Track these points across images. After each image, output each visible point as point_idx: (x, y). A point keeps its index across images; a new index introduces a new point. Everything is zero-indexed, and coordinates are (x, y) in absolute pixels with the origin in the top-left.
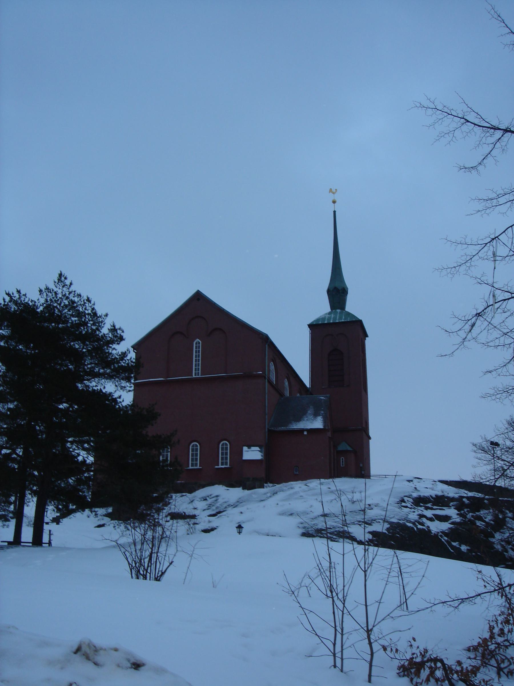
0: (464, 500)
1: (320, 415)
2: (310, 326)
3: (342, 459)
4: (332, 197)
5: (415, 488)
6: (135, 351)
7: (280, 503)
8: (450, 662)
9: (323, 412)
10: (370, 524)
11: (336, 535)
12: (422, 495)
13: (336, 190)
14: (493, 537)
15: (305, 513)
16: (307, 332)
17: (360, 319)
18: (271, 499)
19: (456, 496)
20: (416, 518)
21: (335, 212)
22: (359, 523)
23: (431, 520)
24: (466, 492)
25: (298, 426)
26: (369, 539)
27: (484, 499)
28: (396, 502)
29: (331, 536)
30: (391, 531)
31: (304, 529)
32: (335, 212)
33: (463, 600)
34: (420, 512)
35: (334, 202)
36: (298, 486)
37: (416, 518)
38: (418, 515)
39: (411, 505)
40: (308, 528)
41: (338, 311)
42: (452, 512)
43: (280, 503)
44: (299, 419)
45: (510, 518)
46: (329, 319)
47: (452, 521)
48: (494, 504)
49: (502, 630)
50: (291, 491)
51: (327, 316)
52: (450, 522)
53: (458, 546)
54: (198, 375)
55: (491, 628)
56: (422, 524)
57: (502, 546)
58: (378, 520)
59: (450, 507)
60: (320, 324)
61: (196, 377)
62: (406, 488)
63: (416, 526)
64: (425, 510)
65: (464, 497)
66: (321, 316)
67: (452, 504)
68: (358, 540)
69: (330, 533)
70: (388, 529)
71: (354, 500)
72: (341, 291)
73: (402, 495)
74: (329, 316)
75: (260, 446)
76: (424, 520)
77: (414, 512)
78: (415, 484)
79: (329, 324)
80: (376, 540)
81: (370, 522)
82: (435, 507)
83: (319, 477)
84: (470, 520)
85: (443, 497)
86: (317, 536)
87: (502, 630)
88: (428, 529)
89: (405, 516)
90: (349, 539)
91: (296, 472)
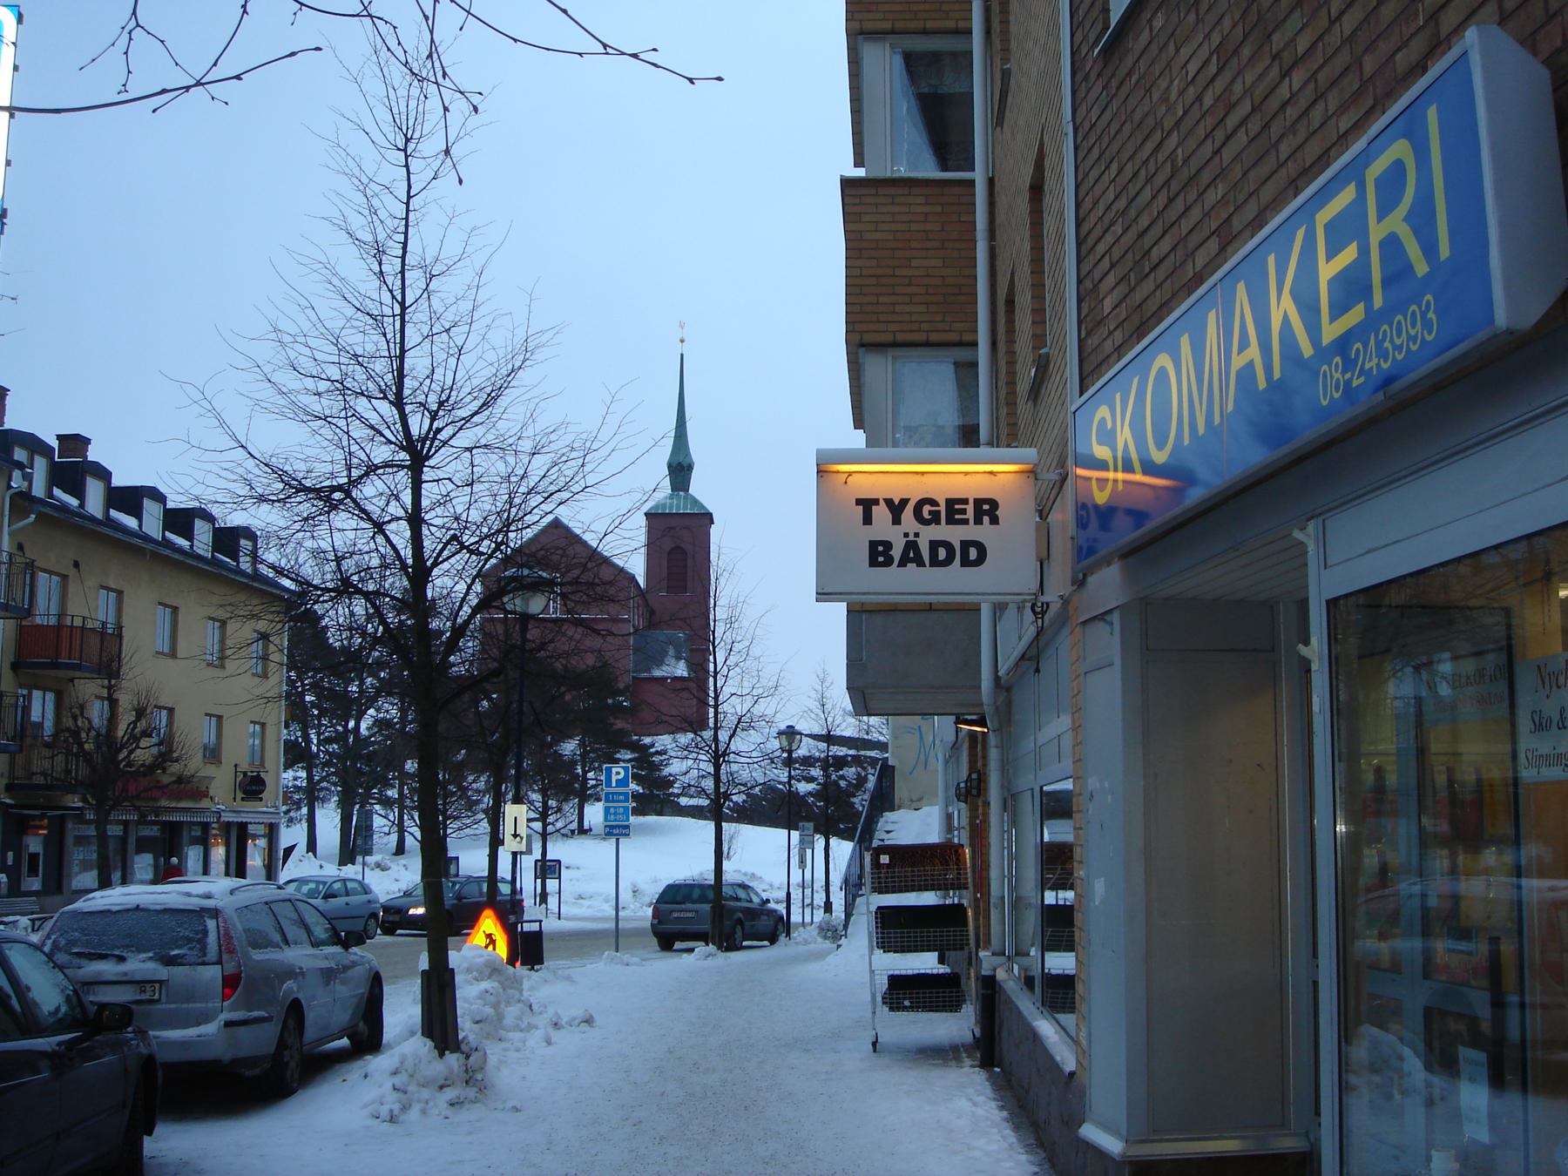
21: (682, 355)
27: (847, 756)
32: (682, 355)
35: (682, 341)
46: (671, 507)
51: (668, 501)
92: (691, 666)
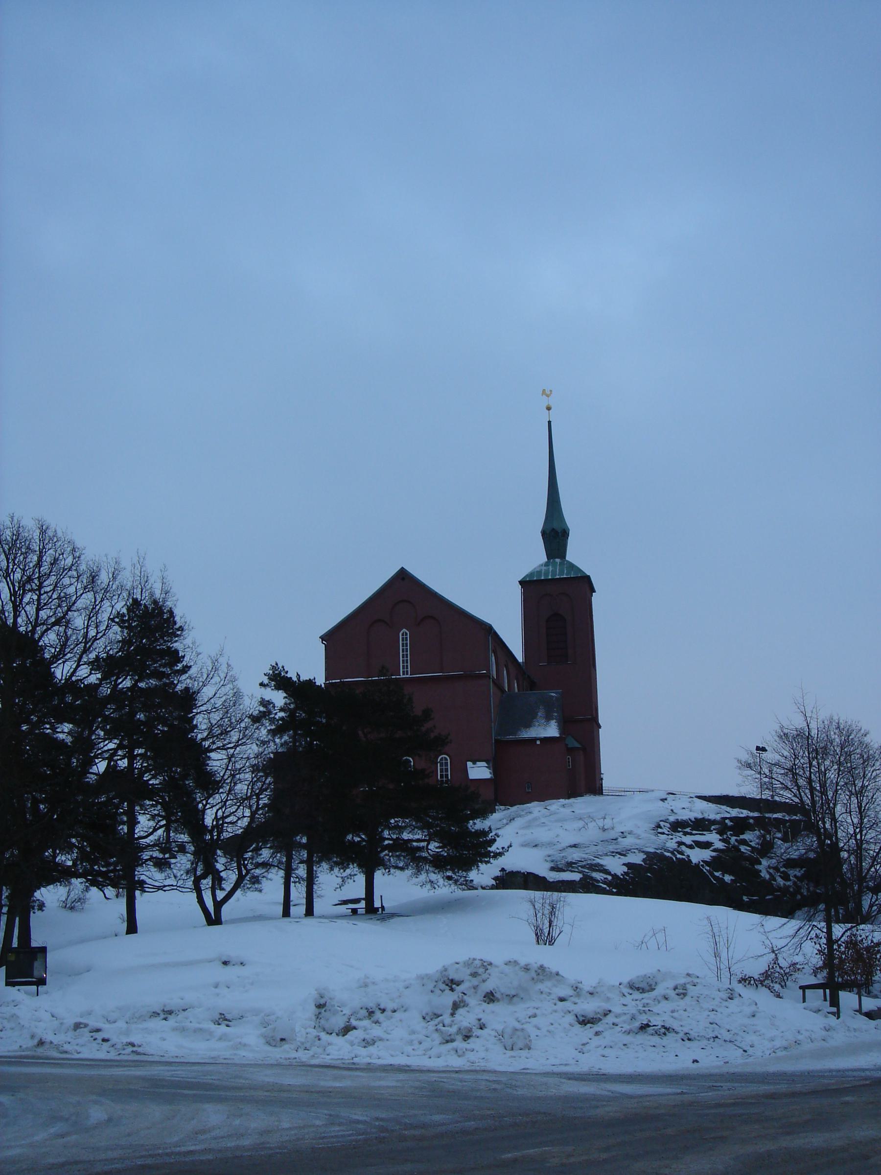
0: (727, 821)
1: (553, 719)
2: (521, 582)
3: (569, 758)
4: (545, 402)
5: (672, 810)
6: (324, 642)
7: (521, 832)
8: (756, 978)
9: (556, 714)
10: (625, 855)
11: (588, 869)
12: (680, 818)
13: (551, 391)
14: (760, 863)
15: (550, 844)
16: (518, 590)
17: (588, 574)
18: (507, 826)
19: (718, 817)
20: (675, 846)
21: (549, 422)
22: (613, 854)
23: (690, 847)
24: (728, 809)
25: (529, 733)
26: (624, 872)
27: (748, 817)
28: (651, 828)
29: (582, 869)
30: (648, 862)
31: (552, 863)
32: (549, 422)
33: (759, 956)
34: (679, 839)
35: (549, 409)
36: (536, 808)
37: (675, 846)
38: (676, 843)
39: (669, 831)
40: (557, 862)
41: (558, 560)
42: (713, 837)
43: (520, 832)
44: (528, 725)
45: (779, 838)
46: (546, 574)
47: (713, 848)
48: (760, 823)
49: (773, 967)
50: (530, 817)
51: (544, 568)
52: (712, 848)
53: (721, 877)
54: (407, 674)
55: (769, 966)
56: (682, 853)
57: (770, 874)
58: (633, 850)
59: (712, 831)
60: (536, 580)
61: (404, 676)
62: (660, 810)
63: (675, 856)
64: (683, 836)
65: (726, 818)
66: (535, 568)
67: (713, 827)
68: (612, 873)
69: (582, 867)
70: (644, 860)
71: (605, 827)
72: (560, 534)
73: (658, 819)
74: (545, 568)
75: (487, 761)
76: (683, 848)
77: (672, 839)
78: (670, 804)
79: (546, 581)
80: (632, 873)
81: (624, 853)
82: (694, 832)
83: (558, 797)
84: (734, 846)
85: (703, 819)
86: (567, 870)
87: (773, 967)
88: (688, 859)
89: (663, 844)
90: (603, 873)
91: (528, 788)
92: (564, 726)
